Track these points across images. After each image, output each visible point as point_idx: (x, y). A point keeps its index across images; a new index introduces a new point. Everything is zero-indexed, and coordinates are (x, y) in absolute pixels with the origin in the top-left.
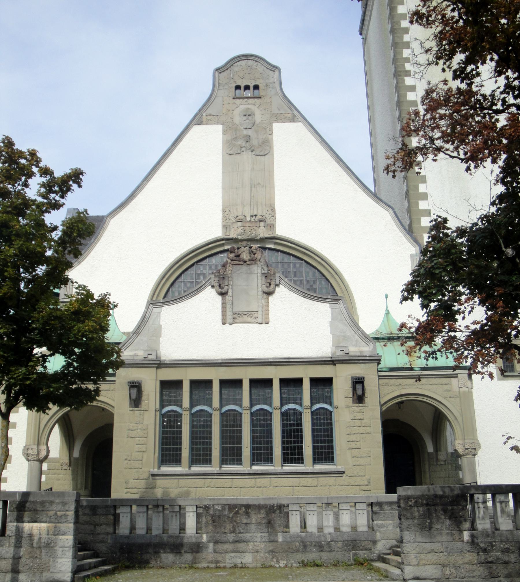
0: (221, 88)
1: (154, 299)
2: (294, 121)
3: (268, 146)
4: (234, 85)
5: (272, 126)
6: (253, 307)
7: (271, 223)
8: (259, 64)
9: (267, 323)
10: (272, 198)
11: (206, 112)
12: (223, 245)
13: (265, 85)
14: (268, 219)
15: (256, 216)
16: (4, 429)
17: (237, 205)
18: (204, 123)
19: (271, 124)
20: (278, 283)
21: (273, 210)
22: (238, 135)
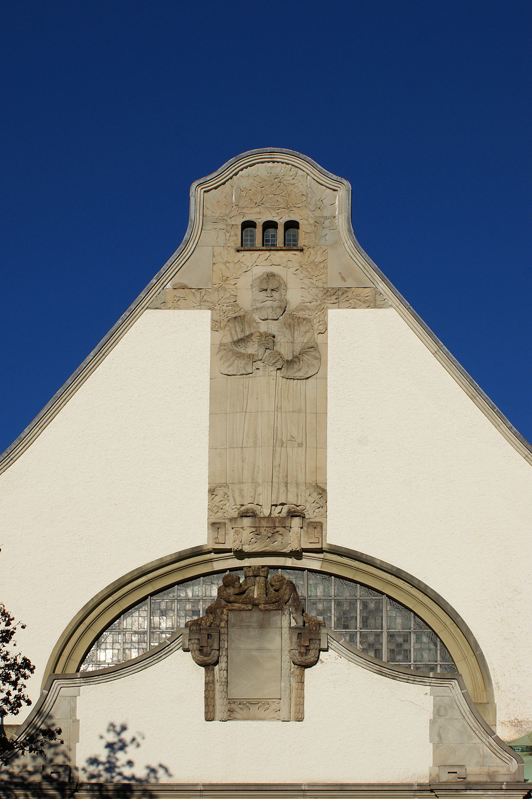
0: (208, 227)
1: (58, 671)
3: (316, 358)
5: (326, 315)
6: (269, 690)
8: (300, 172)
9: (301, 720)
10: (320, 469)
11: (176, 280)
12: (211, 561)
13: (312, 221)
14: (311, 512)
15: (283, 504)
17: (242, 483)
19: (324, 311)
20: (324, 646)
21: (322, 492)
22: (247, 333)
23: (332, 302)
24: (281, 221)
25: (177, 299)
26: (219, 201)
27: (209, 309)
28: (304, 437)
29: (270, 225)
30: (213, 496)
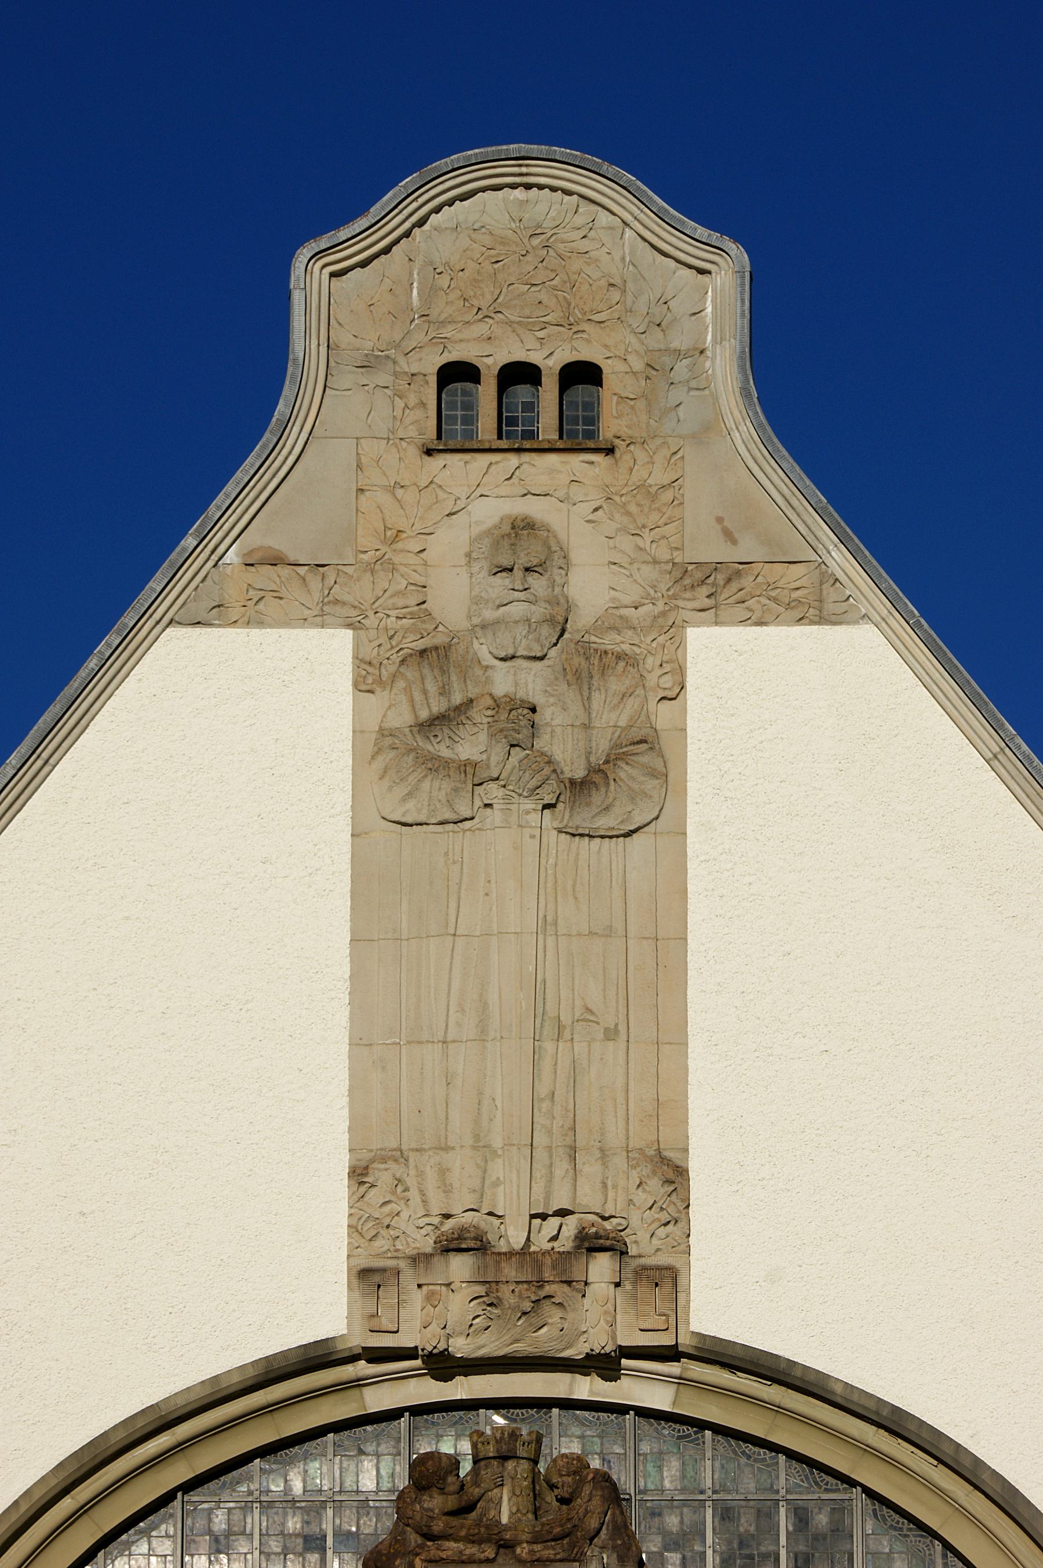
0: (346, 378)
2: (821, 620)
3: (653, 774)
4: (432, 362)
5: (681, 644)
7: (662, 1260)
8: (604, 218)
10: (669, 1106)
13: (638, 365)
14: (643, 1236)
15: (562, 1213)
16: (260, 1369)
17: (447, 1149)
18: (234, 614)
19: (673, 631)
21: (675, 1176)
22: (457, 699)
23: (697, 604)
24: (551, 362)
25: (255, 595)
26: (374, 302)
27: (349, 626)
28: (622, 1010)
29: (519, 375)
30: (363, 1189)
